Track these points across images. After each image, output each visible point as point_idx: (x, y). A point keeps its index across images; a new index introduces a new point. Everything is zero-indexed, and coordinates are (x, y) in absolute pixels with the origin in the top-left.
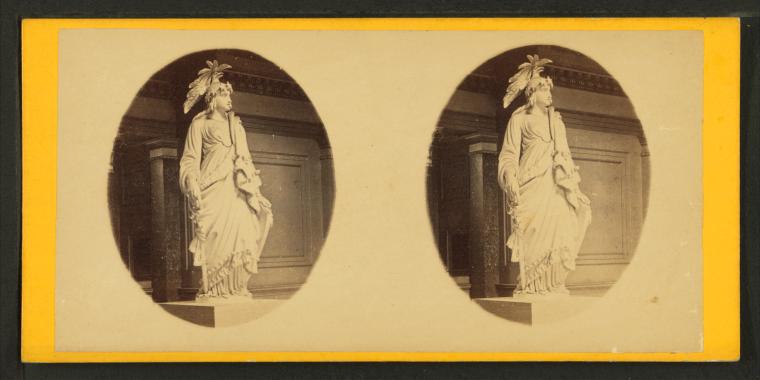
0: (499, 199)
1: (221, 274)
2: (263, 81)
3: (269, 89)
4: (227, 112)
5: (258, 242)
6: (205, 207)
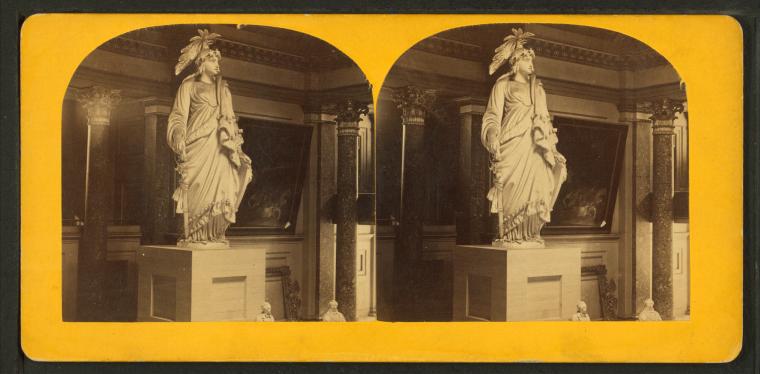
0: (484, 160)
1: (517, 221)
2: (137, 45)
3: (274, 60)
4: (215, 76)
5: (552, 194)
6: (503, 160)
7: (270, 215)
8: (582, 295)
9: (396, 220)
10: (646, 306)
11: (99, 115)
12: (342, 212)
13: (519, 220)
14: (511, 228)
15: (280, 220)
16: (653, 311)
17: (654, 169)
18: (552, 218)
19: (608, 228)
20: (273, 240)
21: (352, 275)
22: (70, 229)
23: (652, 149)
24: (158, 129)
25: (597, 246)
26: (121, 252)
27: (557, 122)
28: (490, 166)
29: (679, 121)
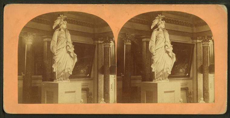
1: (160, 74)
5: (171, 65)
7: (182, 71)
8: (181, 96)
9: (123, 74)
10: (102, 100)
11: (29, 41)
12: (104, 71)
13: (161, 74)
14: (158, 76)
15: (185, 73)
16: (104, 102)
17: (104, 59)
18: (171, 73)
19: (189, 76)
20: (183, 79)
21: (109, 91)
22: (20, 77)
23: (103, 52)
24: (146, 45)
25: (186, 81)
26: (36, 83)
27: (172, 43)
28: (152, 57)
29: (211, 42)
